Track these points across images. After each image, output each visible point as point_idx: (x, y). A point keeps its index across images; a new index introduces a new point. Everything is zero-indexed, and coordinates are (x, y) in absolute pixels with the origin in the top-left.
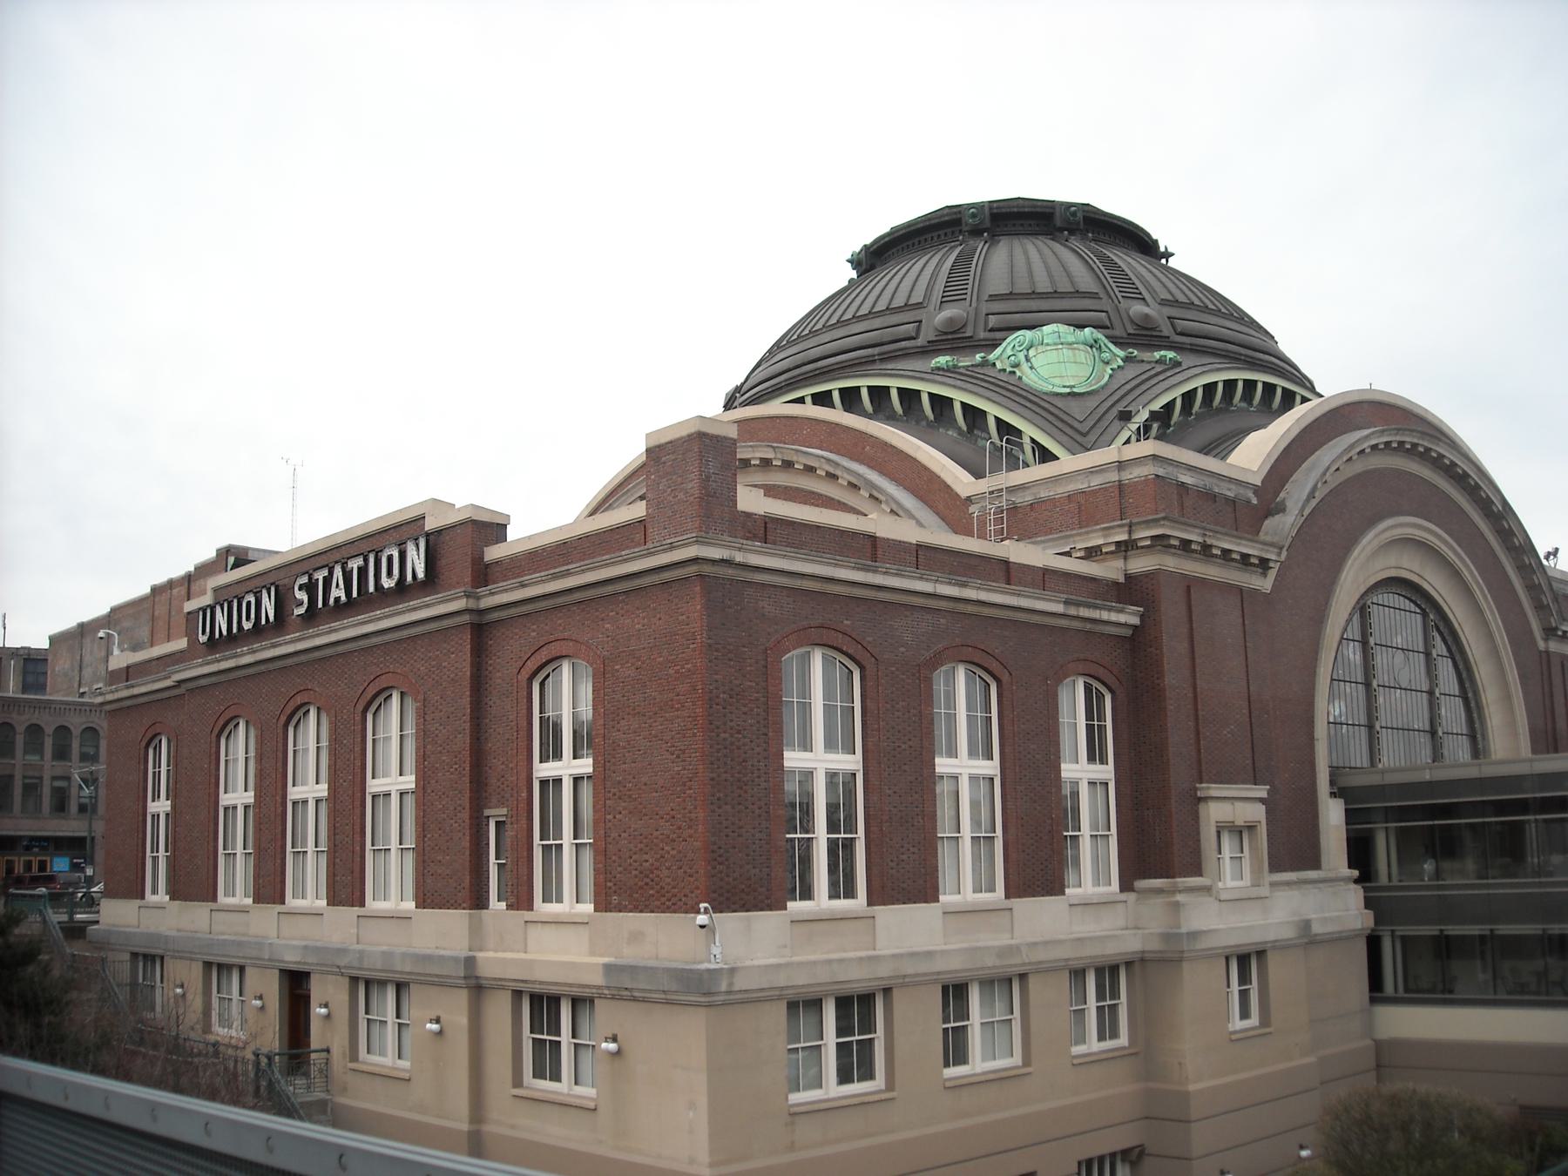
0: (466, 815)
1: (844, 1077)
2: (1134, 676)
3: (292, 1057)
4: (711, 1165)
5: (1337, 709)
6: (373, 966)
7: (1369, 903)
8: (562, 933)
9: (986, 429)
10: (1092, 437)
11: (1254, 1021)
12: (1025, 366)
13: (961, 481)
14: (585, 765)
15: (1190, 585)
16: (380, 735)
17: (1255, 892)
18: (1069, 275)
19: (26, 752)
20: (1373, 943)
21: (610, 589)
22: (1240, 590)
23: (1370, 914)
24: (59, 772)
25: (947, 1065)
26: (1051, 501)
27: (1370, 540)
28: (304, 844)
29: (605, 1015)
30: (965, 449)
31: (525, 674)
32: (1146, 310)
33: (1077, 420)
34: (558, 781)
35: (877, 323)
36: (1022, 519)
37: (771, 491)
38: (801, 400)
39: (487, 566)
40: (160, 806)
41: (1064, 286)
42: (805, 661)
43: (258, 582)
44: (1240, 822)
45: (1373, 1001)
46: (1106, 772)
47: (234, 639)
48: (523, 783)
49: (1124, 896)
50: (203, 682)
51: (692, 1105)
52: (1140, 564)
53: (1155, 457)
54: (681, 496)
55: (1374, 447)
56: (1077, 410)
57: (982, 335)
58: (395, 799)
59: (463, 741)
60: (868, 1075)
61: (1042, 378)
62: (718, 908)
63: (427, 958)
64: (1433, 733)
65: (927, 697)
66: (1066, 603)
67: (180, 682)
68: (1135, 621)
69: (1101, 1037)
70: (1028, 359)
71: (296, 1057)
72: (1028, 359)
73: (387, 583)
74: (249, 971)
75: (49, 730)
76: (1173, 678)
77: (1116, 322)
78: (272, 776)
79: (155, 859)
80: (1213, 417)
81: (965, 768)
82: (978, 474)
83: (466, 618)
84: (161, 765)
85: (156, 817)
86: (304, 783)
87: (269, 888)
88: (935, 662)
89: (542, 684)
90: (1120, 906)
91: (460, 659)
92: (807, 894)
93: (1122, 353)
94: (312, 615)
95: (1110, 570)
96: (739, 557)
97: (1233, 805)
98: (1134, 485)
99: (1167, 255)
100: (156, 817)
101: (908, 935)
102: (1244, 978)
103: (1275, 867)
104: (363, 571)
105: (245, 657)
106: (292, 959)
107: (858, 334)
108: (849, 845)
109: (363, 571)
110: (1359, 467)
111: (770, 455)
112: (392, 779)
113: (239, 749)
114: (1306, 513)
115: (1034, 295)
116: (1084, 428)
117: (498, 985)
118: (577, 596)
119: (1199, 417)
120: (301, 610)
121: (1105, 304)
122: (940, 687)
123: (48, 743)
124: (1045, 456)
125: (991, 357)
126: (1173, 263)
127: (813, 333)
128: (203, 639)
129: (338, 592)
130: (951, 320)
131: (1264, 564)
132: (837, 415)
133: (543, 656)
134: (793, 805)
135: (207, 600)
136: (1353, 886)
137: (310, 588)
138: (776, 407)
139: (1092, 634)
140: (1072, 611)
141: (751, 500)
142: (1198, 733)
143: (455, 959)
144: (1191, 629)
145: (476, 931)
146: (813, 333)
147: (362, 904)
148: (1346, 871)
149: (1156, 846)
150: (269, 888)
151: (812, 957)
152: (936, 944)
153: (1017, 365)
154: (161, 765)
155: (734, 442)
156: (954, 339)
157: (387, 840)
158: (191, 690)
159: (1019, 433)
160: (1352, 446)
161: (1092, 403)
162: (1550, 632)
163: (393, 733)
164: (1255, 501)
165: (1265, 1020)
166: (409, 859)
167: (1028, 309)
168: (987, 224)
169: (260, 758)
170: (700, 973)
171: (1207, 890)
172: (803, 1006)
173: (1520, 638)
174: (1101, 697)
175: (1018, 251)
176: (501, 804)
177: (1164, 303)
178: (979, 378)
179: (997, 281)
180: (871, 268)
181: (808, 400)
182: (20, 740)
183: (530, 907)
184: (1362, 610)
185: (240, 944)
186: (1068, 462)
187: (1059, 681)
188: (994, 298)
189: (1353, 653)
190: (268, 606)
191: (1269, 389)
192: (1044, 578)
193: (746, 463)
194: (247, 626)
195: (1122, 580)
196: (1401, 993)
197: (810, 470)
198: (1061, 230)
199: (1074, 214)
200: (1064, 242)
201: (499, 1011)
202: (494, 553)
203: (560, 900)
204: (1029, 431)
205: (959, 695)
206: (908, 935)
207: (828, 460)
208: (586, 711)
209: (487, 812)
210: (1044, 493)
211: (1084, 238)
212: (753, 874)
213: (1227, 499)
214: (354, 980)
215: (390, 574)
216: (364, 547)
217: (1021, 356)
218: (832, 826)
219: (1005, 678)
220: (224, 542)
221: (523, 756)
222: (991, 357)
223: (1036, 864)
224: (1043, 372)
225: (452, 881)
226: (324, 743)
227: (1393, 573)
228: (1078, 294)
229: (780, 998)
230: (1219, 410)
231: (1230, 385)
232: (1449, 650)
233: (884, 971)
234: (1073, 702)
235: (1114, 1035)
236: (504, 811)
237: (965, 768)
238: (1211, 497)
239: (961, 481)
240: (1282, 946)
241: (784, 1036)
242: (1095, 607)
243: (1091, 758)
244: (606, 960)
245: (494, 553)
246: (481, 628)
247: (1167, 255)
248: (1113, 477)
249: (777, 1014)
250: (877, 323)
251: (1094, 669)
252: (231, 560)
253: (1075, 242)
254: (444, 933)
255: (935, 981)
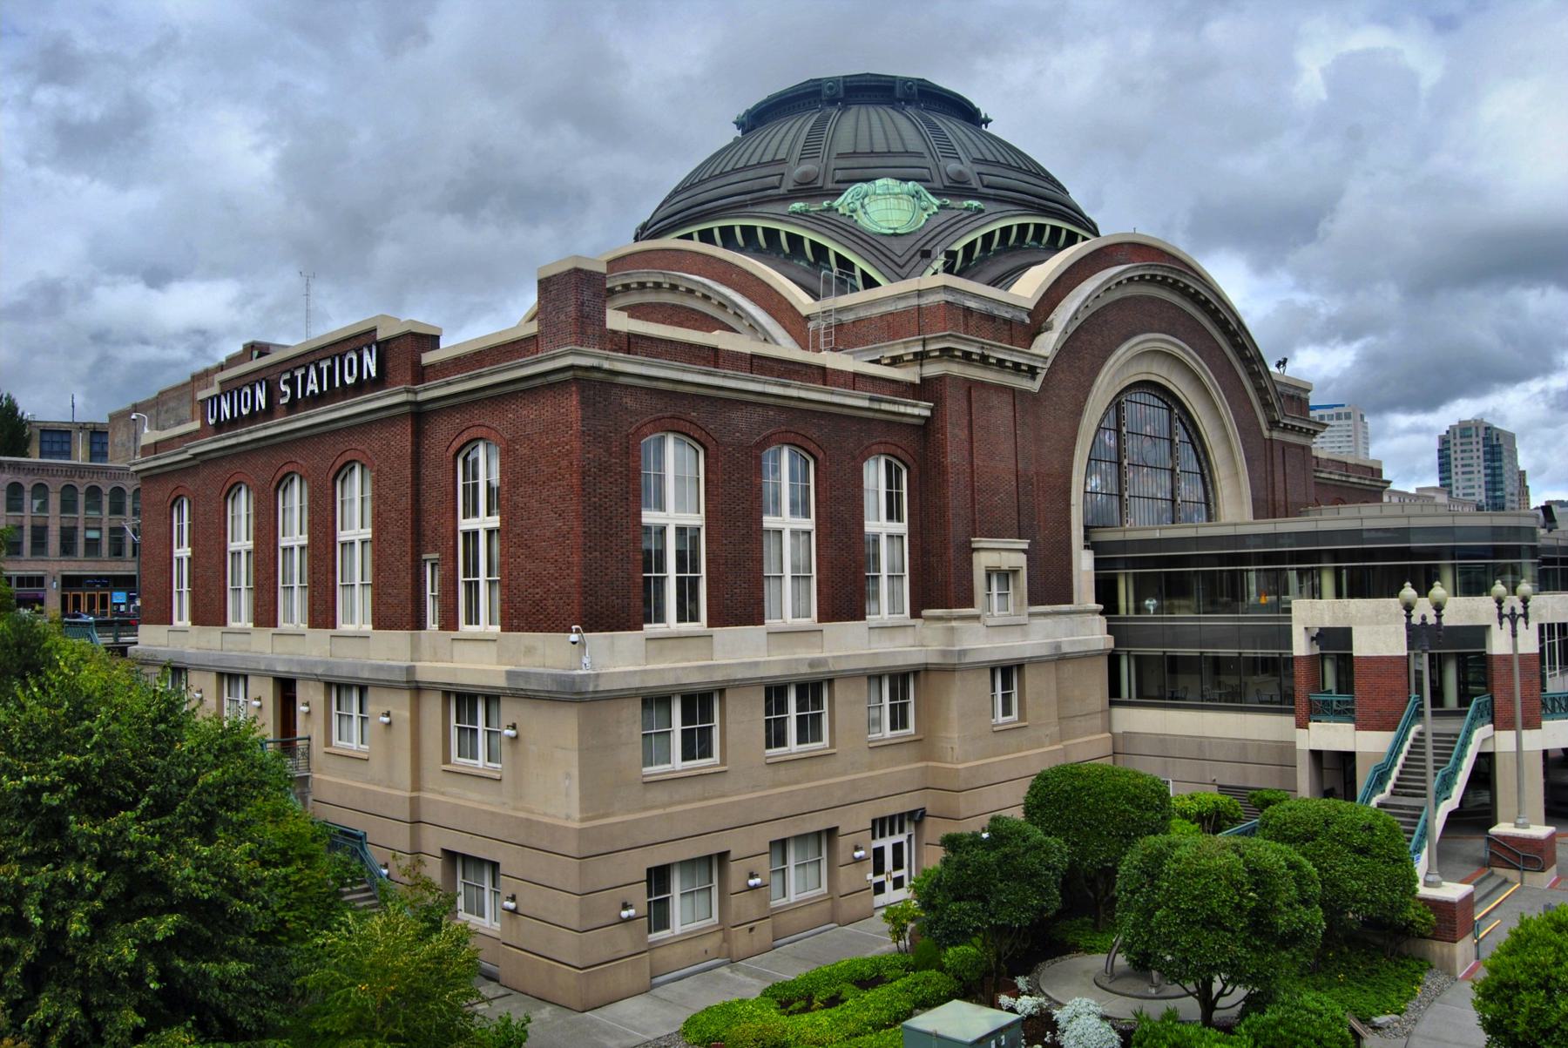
0: (408, 559)
1: (687, 755)
2: (919, 452)
3: (283, 743)
4: (582, 820)
5: (1094, 482)
6: (343, 673)
7: (1110, 630)
8: (479, 651)
9: (828, 262)
10: (907, 269)
11: (1015, 715)
12: (860, 212)
13: (803, 301)
14: (495, 522)
15: (971, 385)
16: (347, 497)
17: (1015, 620)
18: (902, 139)
19: (87, 508)
20: (1113, 660)
21: (511, 388)
22: (1013, 389)
23: (1111, 638)
24: (115, 524)
25: (768, 746)
26: (869, 319)
27: (1123, 352)
28: (292, 581)
29: (509, 711)
30: (809, 280)
31: (452, 451)
32: (960, 167)
33: (901, 254)
34: (476, 533)
35: (750, 174)
36: (845, 334)
37: (635, 311)
38: (689, 237)
39: (425, 368)
40: (183, 552)
41: (897, 147)
42: (661, 444)
43: (253, 377)
44: (1005, 567)
45: (1111, 704)
46: (902, 527)
47: (235, 422)
48: (450, 533)
49: (913, 622)
50: (213, 455)
51: (568, 776)
52: (932, 370)
53: (945, 287)
54: (563, 317)
55: (1130, 280)
56: (898, 247)
57: (830, 185)
58: (358, 546)
59: (406, 502)
60: (707, 753)
61: (876, 223)
62: (589, 627)
63: (380, 668)
64: (1173, 501)
65: (759, 471)
66: (871, 399)
67: (195, 456)
68: (927, 413)
69: (893, 727)
70: (863, 206)
71: (288, 743)
72: (863, 206)
73: (349, 380)
74: (251, 679)
75: (106, 491)
76: (954, 457)
77: (936, 177)
78: (266, 530)
79: (180, 593)
80: (1000, 256)
81: (789, 524)
82: (816, 296)
83: (407, 409)
84: (182, 521)
85: (180, 560)
86: (351, 528)
87: (265, 615)
88: (764, 443)
89: (465, 459)
90: (910, 630)
91: (402, 439)
92: (660, 618)
93: (937, 202)
94: (293, 406)
95: (909, 374)
96: (606, 365)
97: (999, 554)
98: (929, 308)
99: (987, 121)
100: (180, 560)
101: (740, 651)
102: (1007, 685)
103: (1033, 601)
104: (331, 370)
105: (245, 436)
106: (281, 669)
107: (735, 183)
108: (694, 582)
109: (331, 370)
110: (1117, 295)
111: (661, 280)
112: (355, 529)
113: (242, 509)
114: (1070, 331)
115: (872, 153)
116: (901, 261)
117: (432, 687)
118: (489, 393)
119: (997, 253)
120: (284, 401)
121: (929, 162)
122: (769, 464)
123: (106, 501)
124: (870, 283)
125: (835, 204)
126: (990, 129)
127: (702, 182)
128: (211, 421)
129: (313, 387)
130: (805, 174)
131: (1032, 372)
132: (718, 252)
133: (465, 438)
134: (649, 551)
135: (215, 390)
136: (1098, 617)
137: (292, 383)
138: (670, 242)
139: (893, 425)
140: (876, 406)
141: (617, 321)
142: (973, 500)
143: (400, 668)
144: (970, 422)
145: (415, 647)
146: (702, 182)
147: (334, 627)
148: (1093, 605)
149: (939, 585)
150: (265, 615)
151: (662, 666)
152: (762, 657)
153: (854, 211)
154: (182, 521)
155: (603, 276)
156: (808, 189)
157: (352, 577)
158: (204, 462)
159: (852, 265)
160: (1111, 279)
161: (910, 241)
162: (1273, 424)
163: (355, 494)
164: (1028, 321)
165: (1022, 717)
166: (368, 592)
167: (864, 167)
168: (842, 94)
169: (257, 514)
170: (574, 677)
171: (977, 618)
172: (655, 701)
173: (1248, 429)
174: (899, 471)
175: (874, 117)
176: (435, 550)
177: (976, 161)
178: (824, 221)
179: (844, 142)
180: (753, 128)
181: (696, 236)
182: (81, 499)
183: (456, 628)
184: (1117, 405)
185: (244, 658)
186: (887, 289)
187: (865, 459)
188: (841, 156)
189: (1109, 440)
190: (261, 396)
191: (1056, 231)
192: (855, 380)
193: (612, 291)
194: (245, 412)
195: (918, 381)
196: (1134, 699)
197: (690, 292)
198: (900, 101)
199: (910, 88)
200: (901, 111)
201: (433, 706)
202: (428, 358)
203: (477, 623)
204: (860, 264)
205: (784, 472)
206: (740, 651)
207: (704, 285)
208: (496, 480)
209: (425, 556)
210: (862, 314)
211: (918, 107)
212: (620, 604)
213: (1005, 321)
214: (328, 685)
215: (351, 374)
216: (333, 351)
217: (858, 204)
218: (681, 566)
219: (821, 456)
220: (248, 340)
221: (450, 514)
222: (835, 204)
223: (844, 596)
224: (875, 217)
225: (399, 609)
226: (305, 503)
227: (1145, 377)
228: (907, 153)
229: (636, 696)
230: (1013, 248)
231: (1023, 228)
232: (1189, 436)
233: (718, 676)
234: (875, 475)
235: (904, 725)
236: (437, 556)
237: (789, 524)
238: (991, 318)
239: (803, 301)
240: (1037, 661)
241: (639, 725)
242: (895, 403)
243: (890, 517)
244: (508, 668)
245: (428, 358)
246: (419, 416)
247: (987, 121)
248: (914, 302)
249: (634, 710)
250: (764, 171)
251: (893, 449)
252: (256, 353)
253: (910, 111)
254: (391, 650)
255: (760, 684)
